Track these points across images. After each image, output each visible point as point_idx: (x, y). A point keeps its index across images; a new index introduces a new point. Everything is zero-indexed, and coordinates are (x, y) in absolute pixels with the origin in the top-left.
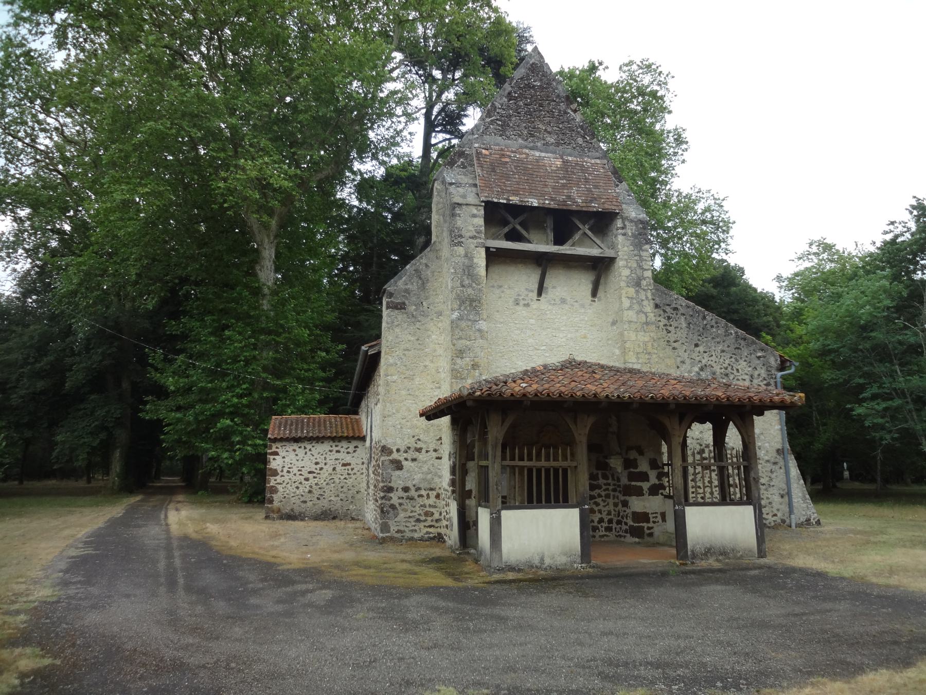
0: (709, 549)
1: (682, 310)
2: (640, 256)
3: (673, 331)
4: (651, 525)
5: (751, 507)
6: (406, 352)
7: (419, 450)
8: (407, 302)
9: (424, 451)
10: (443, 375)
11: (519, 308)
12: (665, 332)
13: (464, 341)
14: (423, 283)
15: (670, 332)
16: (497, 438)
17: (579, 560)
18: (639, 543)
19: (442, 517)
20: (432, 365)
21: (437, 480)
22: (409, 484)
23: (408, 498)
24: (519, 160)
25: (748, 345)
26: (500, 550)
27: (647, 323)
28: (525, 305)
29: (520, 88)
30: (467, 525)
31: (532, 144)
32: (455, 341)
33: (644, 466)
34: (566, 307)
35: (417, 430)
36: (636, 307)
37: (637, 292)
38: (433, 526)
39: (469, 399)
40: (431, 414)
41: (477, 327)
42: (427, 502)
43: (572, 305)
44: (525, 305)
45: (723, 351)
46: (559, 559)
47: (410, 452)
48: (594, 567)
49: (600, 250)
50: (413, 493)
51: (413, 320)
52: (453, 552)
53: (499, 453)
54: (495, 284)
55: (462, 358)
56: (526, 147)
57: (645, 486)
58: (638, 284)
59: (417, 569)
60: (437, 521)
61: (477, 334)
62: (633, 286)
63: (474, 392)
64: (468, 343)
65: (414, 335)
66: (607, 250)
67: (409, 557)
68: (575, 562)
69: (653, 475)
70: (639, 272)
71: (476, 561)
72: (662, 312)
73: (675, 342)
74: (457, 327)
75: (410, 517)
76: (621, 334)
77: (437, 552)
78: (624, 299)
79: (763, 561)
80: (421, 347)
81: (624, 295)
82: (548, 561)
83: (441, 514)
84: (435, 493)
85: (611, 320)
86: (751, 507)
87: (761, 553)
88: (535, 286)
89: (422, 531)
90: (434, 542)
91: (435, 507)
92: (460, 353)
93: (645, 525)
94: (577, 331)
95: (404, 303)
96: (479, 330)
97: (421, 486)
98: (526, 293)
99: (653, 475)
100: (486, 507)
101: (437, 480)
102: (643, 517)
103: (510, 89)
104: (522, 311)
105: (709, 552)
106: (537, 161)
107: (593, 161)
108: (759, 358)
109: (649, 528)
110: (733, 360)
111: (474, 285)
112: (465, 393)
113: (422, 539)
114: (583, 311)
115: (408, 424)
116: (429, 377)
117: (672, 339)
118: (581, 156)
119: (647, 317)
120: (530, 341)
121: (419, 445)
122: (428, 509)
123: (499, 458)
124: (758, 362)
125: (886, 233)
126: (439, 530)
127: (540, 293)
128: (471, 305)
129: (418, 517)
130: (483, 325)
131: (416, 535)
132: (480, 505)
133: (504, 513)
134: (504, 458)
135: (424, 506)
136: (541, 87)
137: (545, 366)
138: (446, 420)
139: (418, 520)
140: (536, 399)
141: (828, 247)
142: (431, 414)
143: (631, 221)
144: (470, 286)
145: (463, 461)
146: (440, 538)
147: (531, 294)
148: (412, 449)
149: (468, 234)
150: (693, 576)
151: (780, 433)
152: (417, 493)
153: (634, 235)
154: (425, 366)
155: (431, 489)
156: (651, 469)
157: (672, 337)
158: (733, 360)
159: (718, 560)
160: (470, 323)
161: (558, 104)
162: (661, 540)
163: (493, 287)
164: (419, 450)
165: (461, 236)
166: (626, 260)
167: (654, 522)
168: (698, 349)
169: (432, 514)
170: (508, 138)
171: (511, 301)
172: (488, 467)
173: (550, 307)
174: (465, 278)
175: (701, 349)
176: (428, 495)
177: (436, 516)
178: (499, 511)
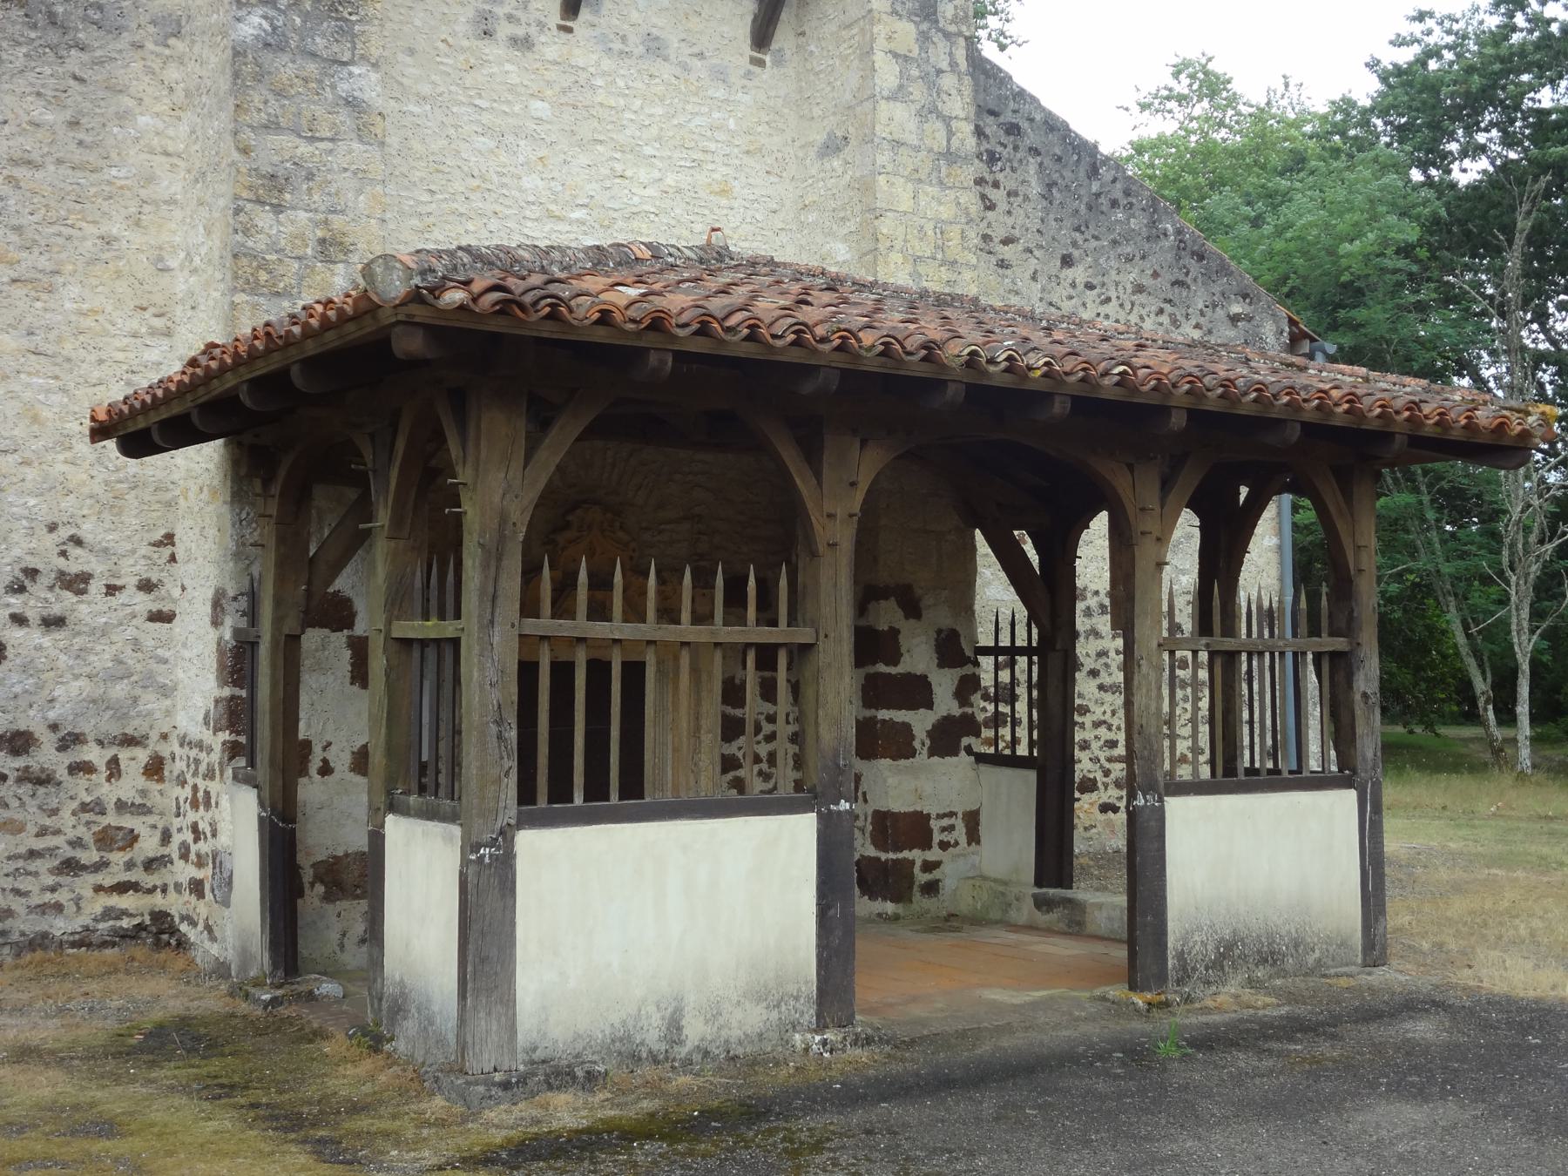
0: (1230, 946)
3: (1002, 206)
4: (934, 854)
5: (1351, 796)
6: (20, 172)
7: (76, 583)
9: (96, 588)
10: (182, 283)
11: (494, 51)
13: (285, 141)
15: (991, 207)
16: (503, 519)
17: (809, 1015)
18: (896, 918)
19: (173, 849)
20: (137, 238)
21: (151, 702)
22: (32, 721)
23: (26, 777)
25: (1208, 277)
26: (509, 1001)
27: (950, 156)
28: (514, 41)
30: (315, 888)
32: (248, 136)
33: (918, 657)
34: (666, 71)
35: (68, 503)
36: (917, 91)
37: (924, 38)
38: (133, 886)
39: (409, 323)
40: (141, 429)
41: (343, 88)
42: (110, 793)
43: (685, 68)
44: (514, 41)
45: (1139, 289)
46: (738, 1014)
47: (38, 589)
48: (869, 1041)
50: (47, 756)
51: (53, 36)
52: (240, 991)
53: (512, 584)
55: (278, 209)
57: (921, 722)
59: (111, 1099)
60: (150, 865)
61: (344, 117)
62: (911, 15)
63: (436, 290)
64: (304, 149)
65: (57, 102)
67: (46, 1032)
68: (794, 1026)
69: (943, 684)
71: (375, 1041)
73: (1006, 241)
74: (259, 78)
75: (32, 854)
76: (865, 187)
77: (161, 995)
78: (879, 58)
79: (1378, 976)
80: (92, 157)
81: (881, 44)
82: (695, 1031)
83: (166, 837)
84: (142, 755)
85: (820, 138)
86: (1351, 796)
87: (1374, 949)
89: (86, 906)
90: (139, 951)
91: (142, 810)
92: (272, 189)
93: (916, 855)
94: (699, 164)
96: (352, 103)
97: (86, 727)
99: (943, 684)
100: (430, 814)
101: (151, 702)
102: (911, 829)
104: (500, 62)
105: (1229, 954)
108: (1234, 319)
109: (929, 867)
110: (1164, 319)
112: (395, 287)
113: (84, 941)
114: (720, 93)
115: (31, 474)
116: (122, 287)
117: (999, 233)
119: (950, 134)
120: (531, 182)
121: (78, 562)
122: (111, 819)
123: (510, 605)
124: (1231, 333)
125: (1399, 42)
126: (158, 901)
129: (68, 852)
130: (364, 82)
131: (60, 926)
132: (393, 808)
133: (532, 845)
134: (529, 608)
135: (98, 807)
137: (655, 250)
138: (200, 463)
139: (71, 867)
140: (701, 346)
141: (1213, 86)
142: (141, 429)
145: (290, 626)
146: (161, 933)
148: (45, 580)
150: (1243, 1060)
151: (1274, 557)
152: (67, 759)
154: (108, 240)
155: (129, 741)
156: (941, 665)
157: (999, 224)
158: (1164, 319)
159: (1252, 983)
160: (312, 68)
162: (965, 906)
164: (76, 583)
167: (944, 846)
168: (1069, 273)
169: (132, 838)
172: (455, 643)
173: (607, 64)
175: (1079, 273)
176: (114, 764)
177: (149, 845)
178: (506, 837)
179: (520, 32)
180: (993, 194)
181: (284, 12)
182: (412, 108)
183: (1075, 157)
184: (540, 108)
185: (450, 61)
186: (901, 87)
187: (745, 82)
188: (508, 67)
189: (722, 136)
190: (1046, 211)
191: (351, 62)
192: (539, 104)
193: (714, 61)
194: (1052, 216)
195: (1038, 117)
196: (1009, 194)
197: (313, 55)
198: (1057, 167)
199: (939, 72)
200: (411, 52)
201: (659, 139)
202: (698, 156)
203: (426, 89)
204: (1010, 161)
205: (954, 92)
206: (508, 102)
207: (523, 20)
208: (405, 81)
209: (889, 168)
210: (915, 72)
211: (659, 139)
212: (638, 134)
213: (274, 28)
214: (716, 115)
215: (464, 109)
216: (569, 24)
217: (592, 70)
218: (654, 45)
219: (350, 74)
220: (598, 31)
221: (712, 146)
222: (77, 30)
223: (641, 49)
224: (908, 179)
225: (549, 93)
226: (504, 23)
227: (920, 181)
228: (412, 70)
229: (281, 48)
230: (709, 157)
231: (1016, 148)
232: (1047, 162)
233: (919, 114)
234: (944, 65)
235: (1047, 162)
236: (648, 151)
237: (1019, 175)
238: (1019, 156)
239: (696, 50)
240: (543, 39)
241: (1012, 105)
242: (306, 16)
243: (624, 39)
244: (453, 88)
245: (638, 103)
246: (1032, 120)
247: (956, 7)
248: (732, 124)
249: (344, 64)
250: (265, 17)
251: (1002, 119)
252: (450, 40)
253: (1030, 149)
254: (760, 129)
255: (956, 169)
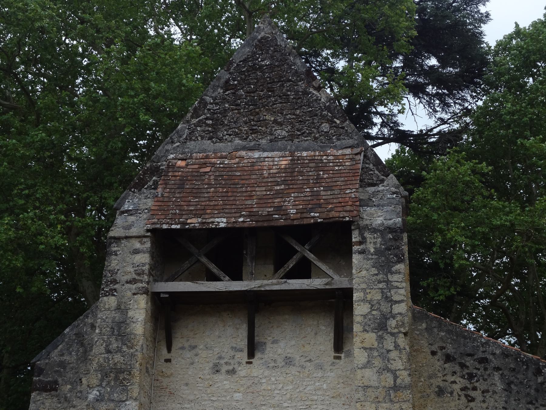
1: (495, 362)
2: (388, 282)
8: (60, 380)
12: (463, 399)
14: (85, 352)
15: (473, 400)
24: (229, 168)
27: (396, 388)
28: (228, 372)
29: (242, 73)
31: (252, 144)
34: (293, 370)
36: (378, 362)
37: (380, 339)
44: (228, 372)
49: (325, 280)
54: (186, 345)
56: (244, 148)
58: (381, 326)
66: (336, 277)
70: (385, 307)
72: (457, 368)
88: (244, 343)
95: (56, 382)
98: (232, 353)
103: (228, 76)
104: (223, 382)
106: (253, 164)
107: (340, 152)
111: (125, 348)
118: (323, 148)
119: (396, 377)
127: (251, 354)
128: (116, 378)
136: (271, 67)
143: (374, 231)
144: (119, 350)
147: (238, 355)
149: (128, 277)
153: (378, 252)
161: (295, 83)
163: (183, 348)
165: (115, 282)
166: (364, 290)
170: (221, 140)
171: (208, 368)
173: (267, 373)
174: (113, 339)
179: (231, 368)
180: (473, 394)
181: (104, 387)
182: (186, 406)
183: (525, 367)
184: (238, 396)
185: (202, 385)
186: (368, 362)
187: (331, 367)
188: (225, 382)
189: (320, 393)
190: (508, 397)
191: (126, 400)
192: (238, 394)
193: (317, 361)
194: (512, 399)
195: (498, 352)
196: (483, 392)
197: (113, 400)
198: (512, 374)
199: (389, 351)
200: (187, 384)
201: (290, 399)
202: (310, 403)
203: (192, 397)
204: (482, 376)
205: (397, 358)
206: (225, 396)
207: (232, 363)
208: (184, 396)
209: (362, 399)
210: (376, 354)
211: (290, 399)
212: (281, 398)
213: (100, 394)
214: (317, 384)
215: (206, 403)
216: (251, 360)
217: (261, 376)
218: (288, 361)
219: (126, 405)
220: (264, 360)
221: (316, 398)
222: (73, 401)
223: (283, 363)
224: (372, 402)
225: (242, 389)
226: (224, 366)
227: (379, 402)
228: (187, 391)
229: (102, 400)
230: (314, 403)
231: (486, 369)
232: (506, 372)
233: (378, 372)
234: (391, 348)
235: (506, 372)
236: (286, 405)
237: (489, 382)
238: (488, 372)
239: (308, 359)
240: (240, 369)
241: (481, 349)
242: (111, 387)
243: (275, 361)
244: (203, 395)
245: (281, 386)
246: (494, 354)
247: (397, 321)
248: (325, 386)
249: (124, 401)
250: (98, 391)
251: (476, 357)
252: (202, 377)
253: (494, 368)
254: (339, 386)
255: (399, 393)
